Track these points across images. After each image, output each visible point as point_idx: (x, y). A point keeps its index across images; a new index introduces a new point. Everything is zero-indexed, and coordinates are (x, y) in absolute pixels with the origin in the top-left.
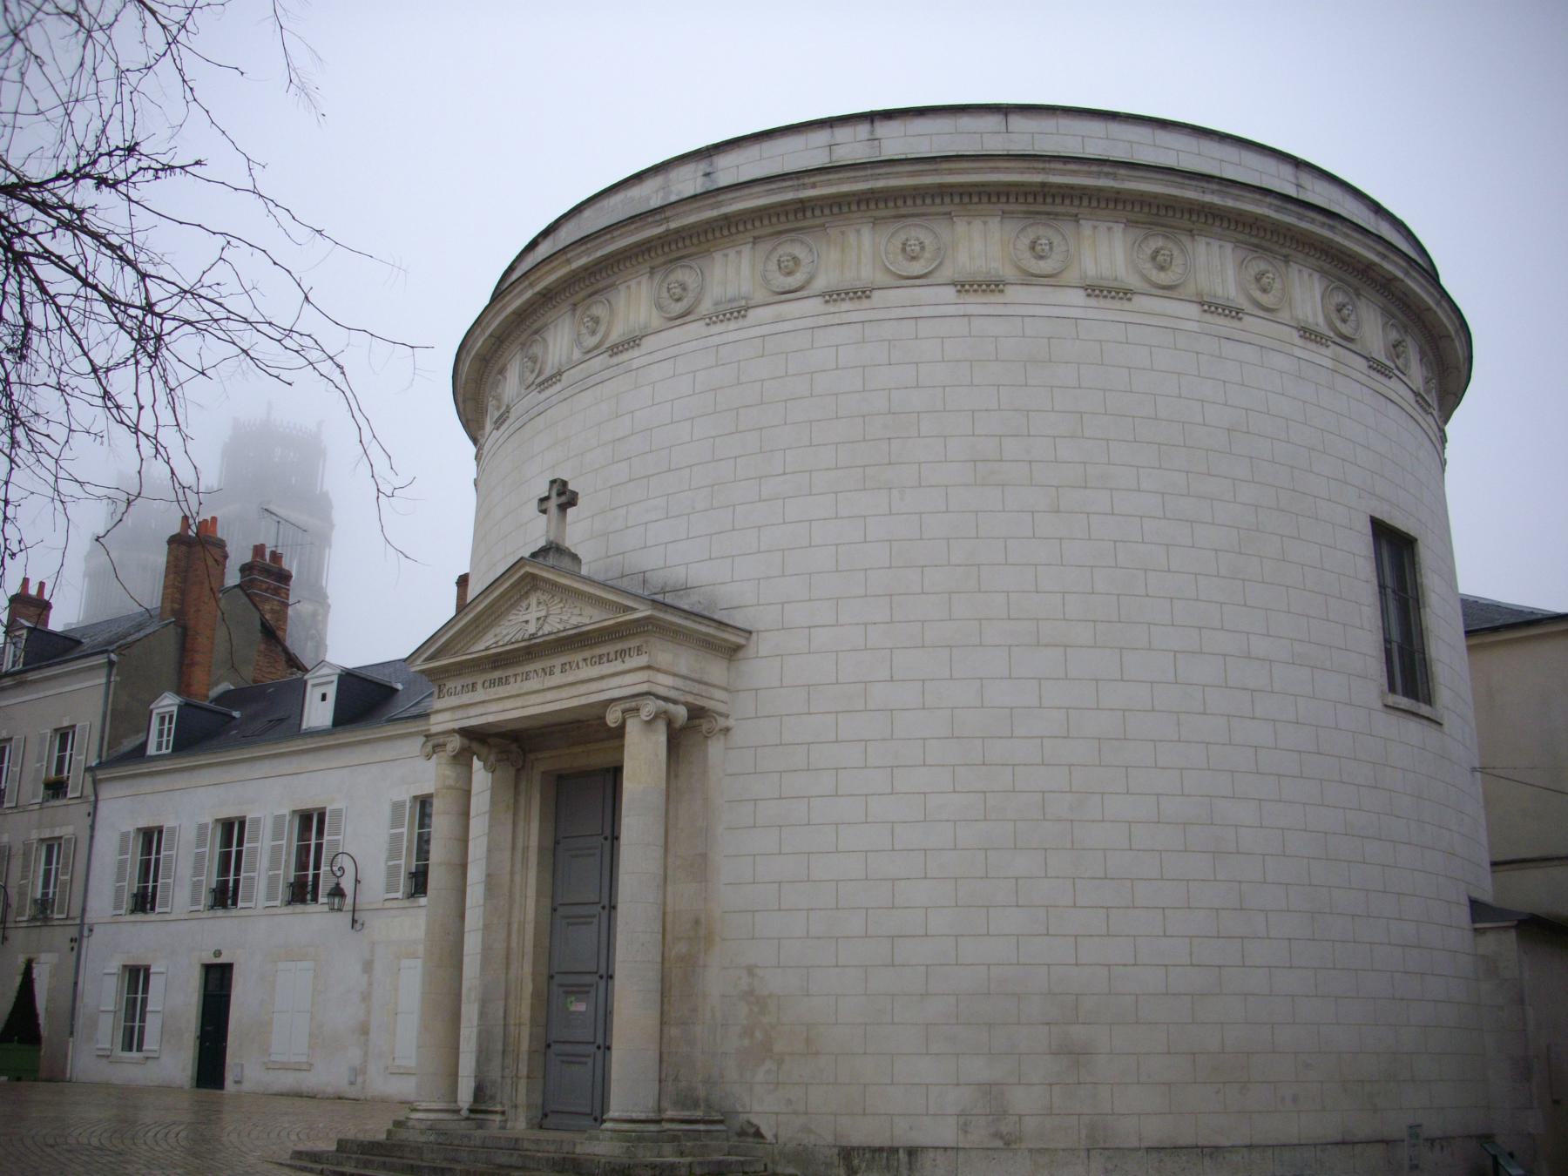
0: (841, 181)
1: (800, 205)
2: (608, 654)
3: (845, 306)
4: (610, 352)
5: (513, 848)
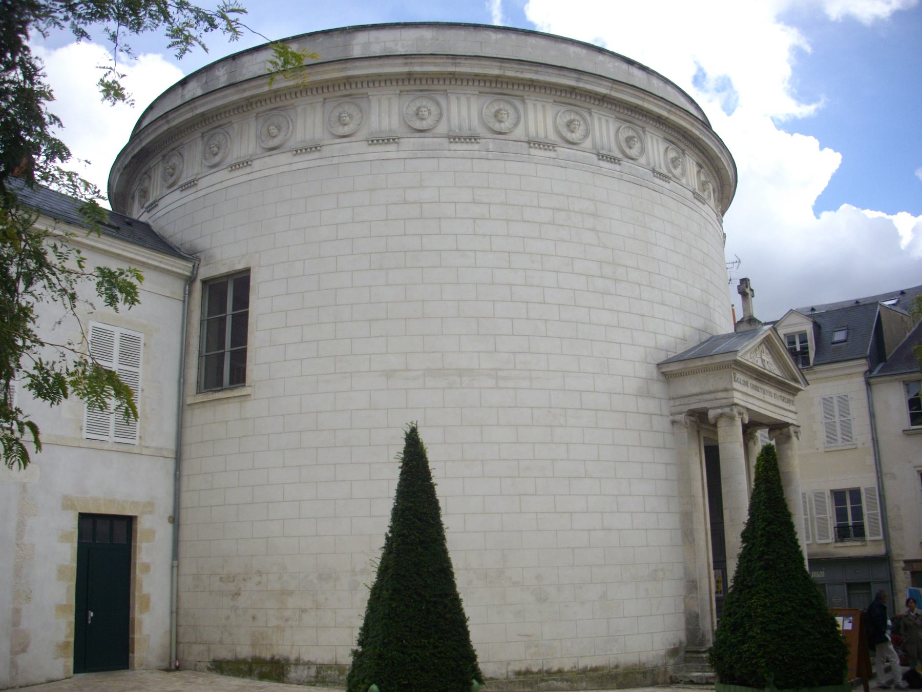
4: (181, 189)
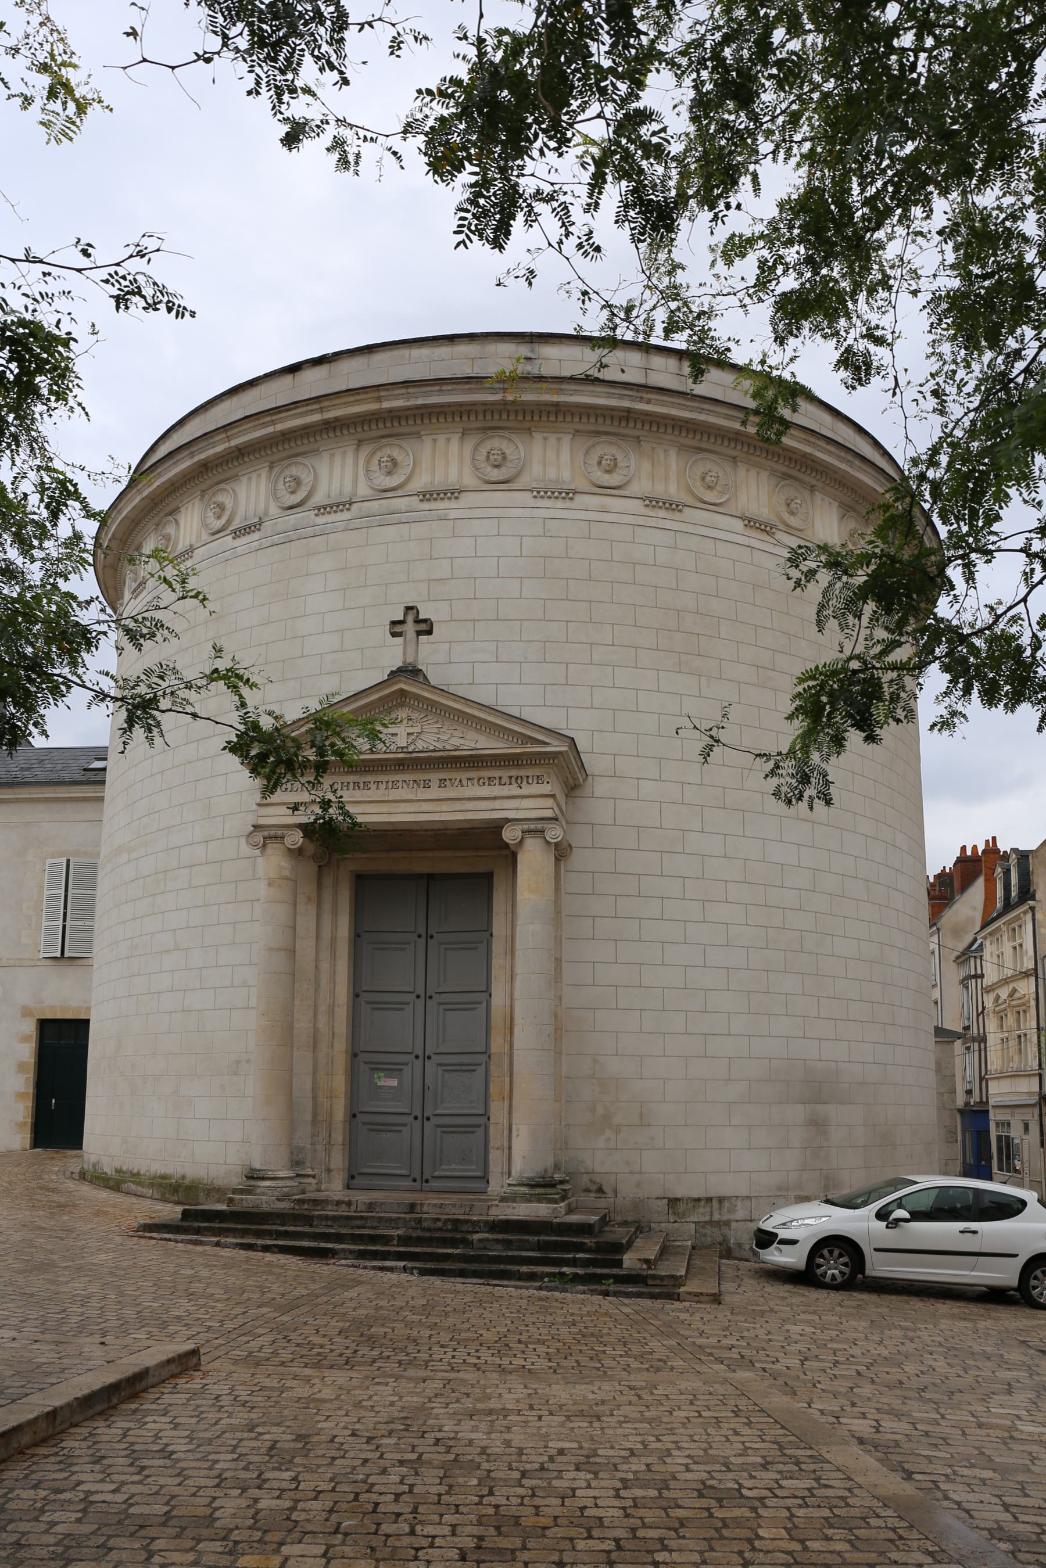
0: (672, 405)
1: (625, 414)
2: (500, 778)
3: (662, 513)
5: (318, 937)
